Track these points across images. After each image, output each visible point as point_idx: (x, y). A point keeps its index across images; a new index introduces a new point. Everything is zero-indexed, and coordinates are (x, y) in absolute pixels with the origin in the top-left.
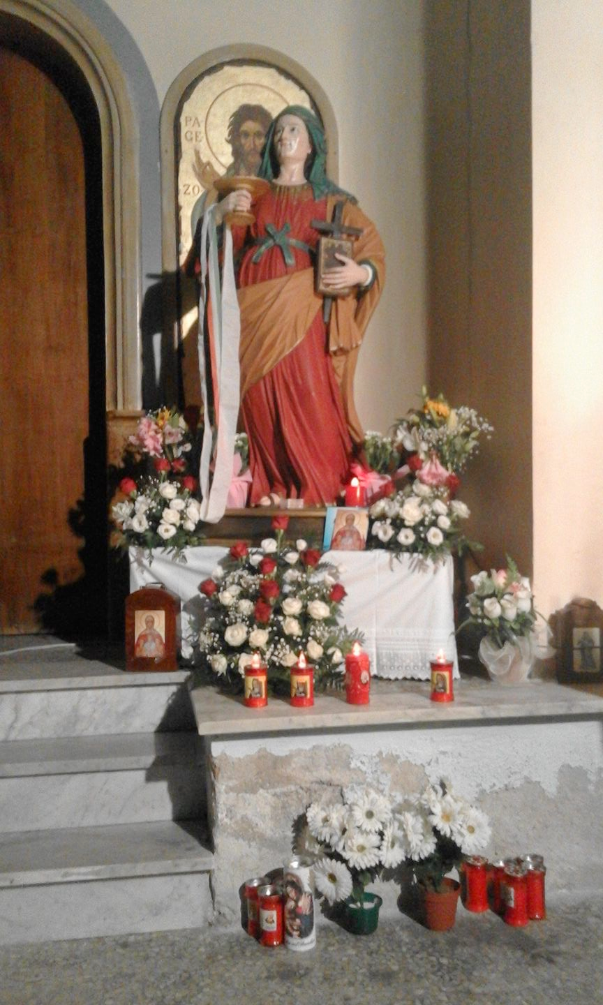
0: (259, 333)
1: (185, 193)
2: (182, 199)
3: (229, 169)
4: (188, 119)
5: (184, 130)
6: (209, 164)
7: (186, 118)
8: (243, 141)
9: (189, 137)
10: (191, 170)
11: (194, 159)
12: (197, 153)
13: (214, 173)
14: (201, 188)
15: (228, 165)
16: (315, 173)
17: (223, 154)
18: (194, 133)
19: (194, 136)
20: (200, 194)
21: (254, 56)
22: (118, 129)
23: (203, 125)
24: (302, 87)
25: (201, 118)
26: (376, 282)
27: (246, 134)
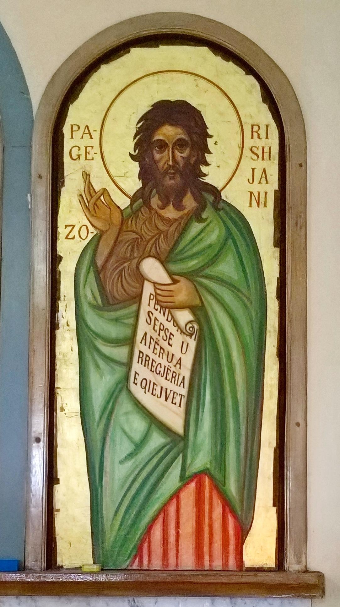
0: (130, 559)
1: (67, 238)
2: (62, 246)
3: (134, 199)
4: (75, 128)
5: (68, 144)
6: (105, 191)
7: (72, 126)
8: (157, 156)
9: (74, 156)
10: (76, 202)
11: (82, 186)
12: (86, 176)
13: (112, 205)
14: (91, 229)
15: (131, 194)
16: (284, 119)
17: (125, 176)
18: (83, 149)
19: (82, 152)
20: (91, 236)
21: (178, 30)
22: (46, 356)
23: (96, 135)
24: (249, 70)
25: (95, 126)
26: (146, 545)
27: (162, 145)
